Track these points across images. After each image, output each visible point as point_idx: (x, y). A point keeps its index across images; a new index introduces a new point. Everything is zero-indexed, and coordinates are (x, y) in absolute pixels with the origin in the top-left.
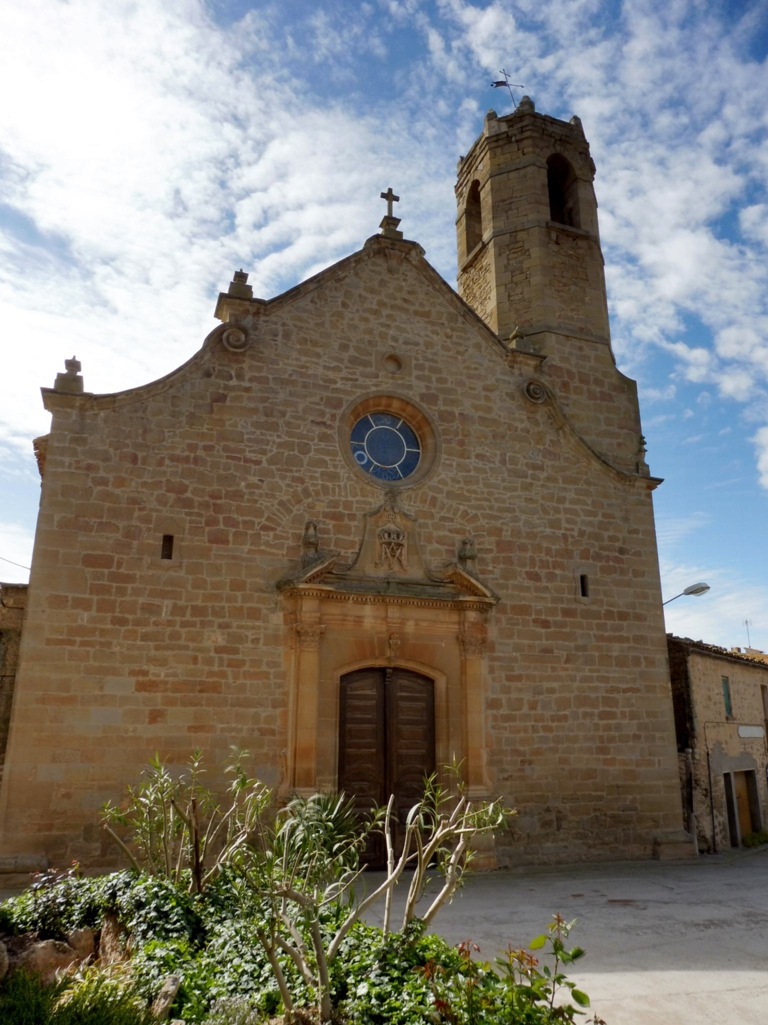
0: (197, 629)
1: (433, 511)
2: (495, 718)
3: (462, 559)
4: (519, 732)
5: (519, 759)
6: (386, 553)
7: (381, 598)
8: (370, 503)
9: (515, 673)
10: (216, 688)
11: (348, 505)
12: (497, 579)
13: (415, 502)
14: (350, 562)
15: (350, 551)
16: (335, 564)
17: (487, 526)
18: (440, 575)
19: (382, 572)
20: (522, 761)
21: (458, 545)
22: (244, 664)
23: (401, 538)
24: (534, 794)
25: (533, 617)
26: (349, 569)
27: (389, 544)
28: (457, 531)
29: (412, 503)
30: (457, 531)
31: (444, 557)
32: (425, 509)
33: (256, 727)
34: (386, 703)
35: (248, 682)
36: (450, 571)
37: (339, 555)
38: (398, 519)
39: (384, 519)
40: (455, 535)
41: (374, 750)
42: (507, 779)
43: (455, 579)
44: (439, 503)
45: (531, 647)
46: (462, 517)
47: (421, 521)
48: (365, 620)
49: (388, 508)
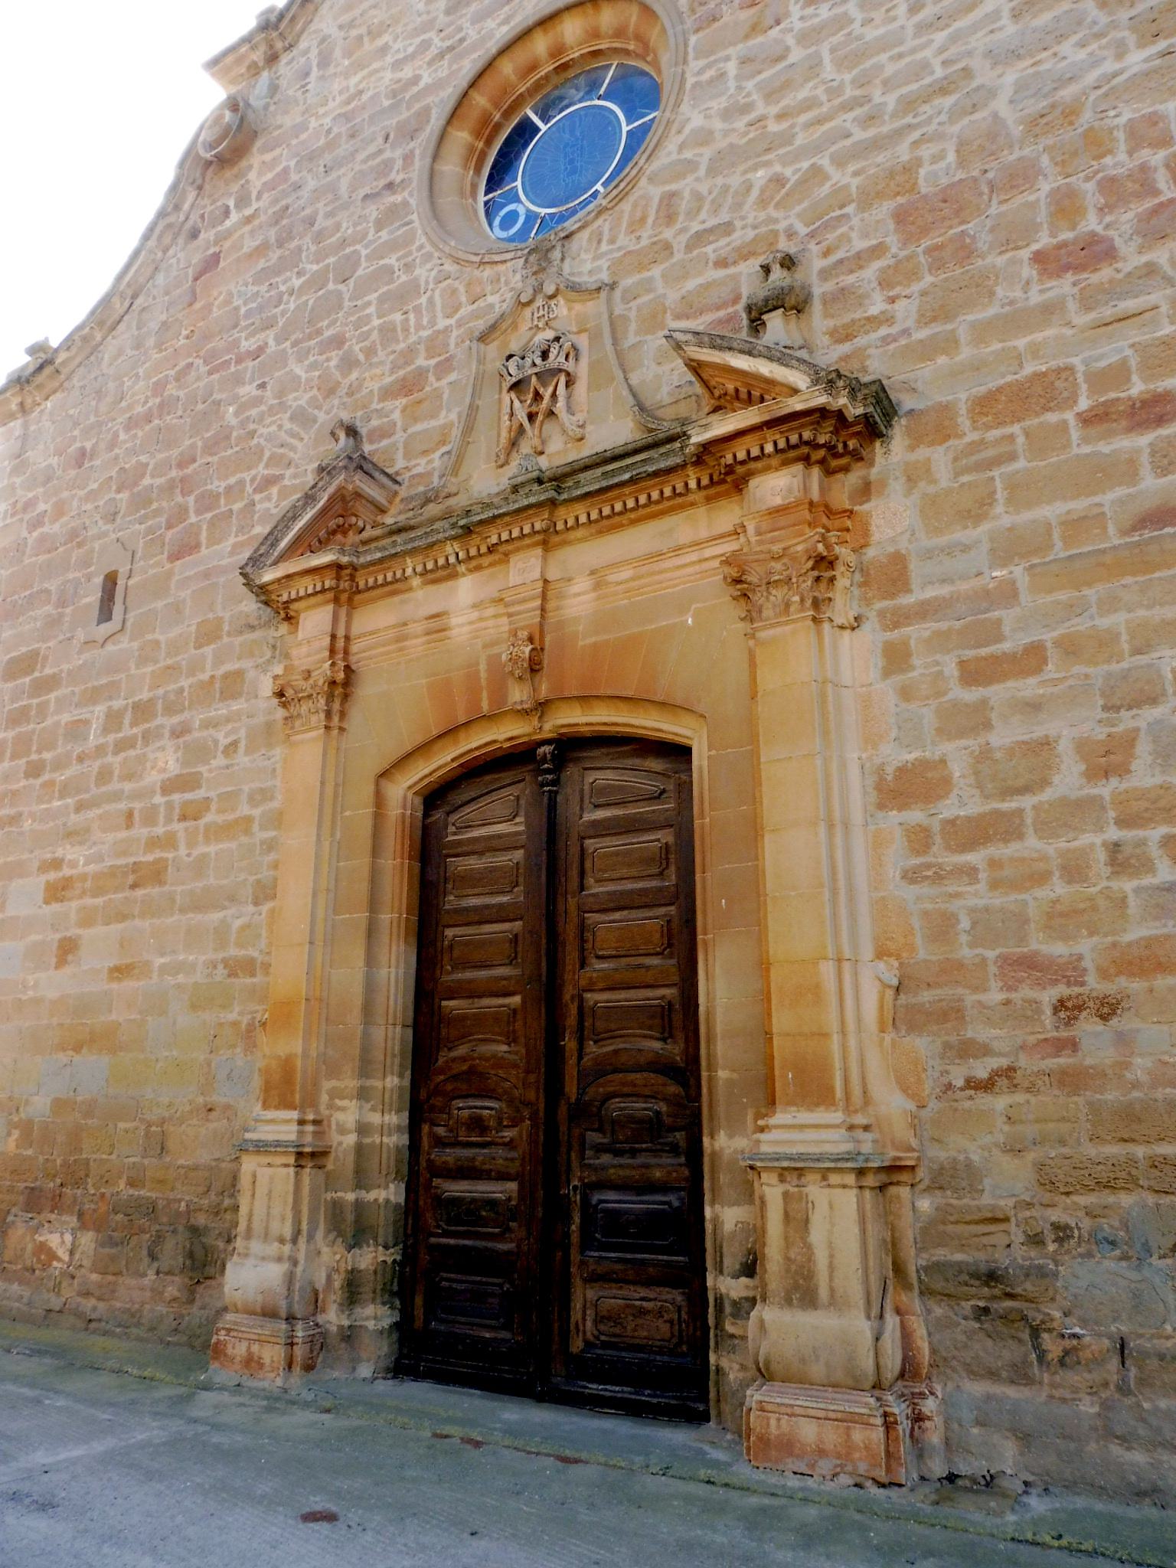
0: (139, 752)
2: (919, 839)
4: (1041, 878)
5: (1048, 996)
9: (1006, 646)
10: (156, 874)
12: (906, 332)
17: (855, 182)
20: (1060, 1005)
22: (208, 809)
24: (1140, 1151)
25: (1084, 404)
33: (220, 955)
34: (554, 856)
35: (212, 849)
41: (516, 1000)
42: (986, 1086)
45: (1075, 526)
48: (454, 621)
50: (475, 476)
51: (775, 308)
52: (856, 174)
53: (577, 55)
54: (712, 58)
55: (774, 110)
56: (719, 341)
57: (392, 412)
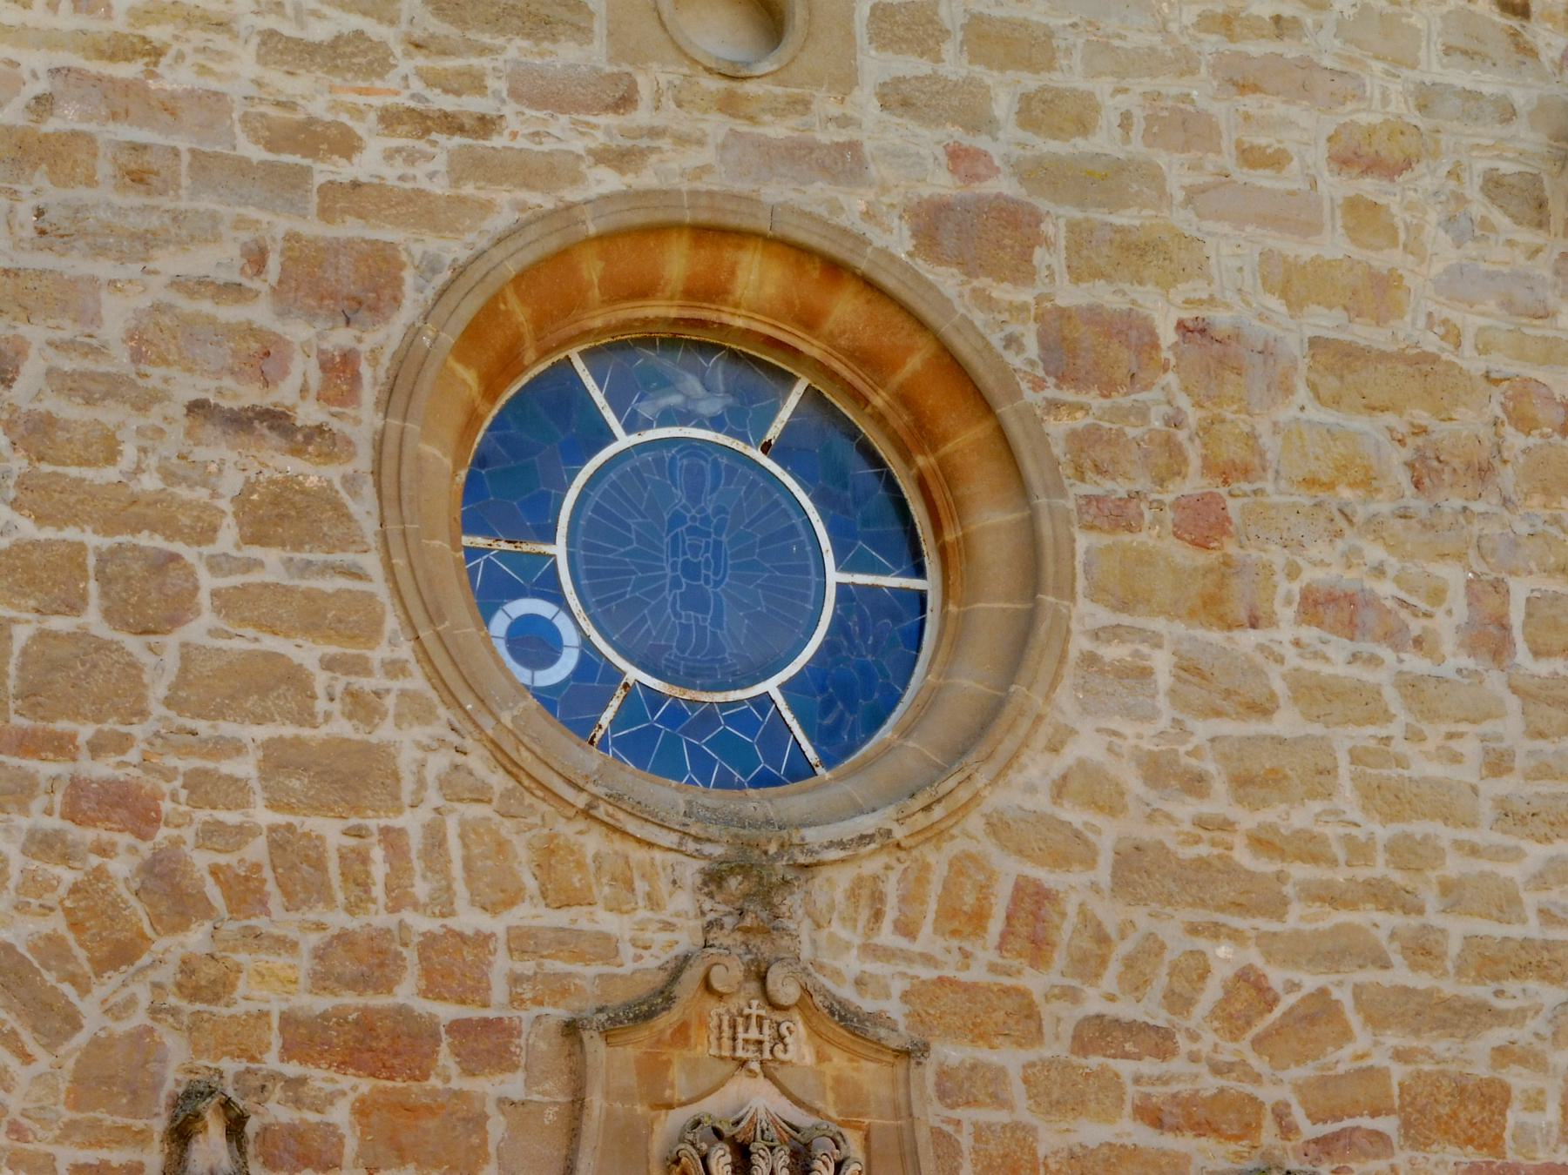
1: (1034, 982)
8: (606, 947)
11: (453, 965)
13: (907, 929)
29: (887, 936)
32: (976, 974)
38: (800, 1048)
39: (705, 1047)
40: (1183, 1143)
46: (1231, 1020)
47: (950, 1052)
49: (728, 975)
52: (1400, 1055)
53: (739, 323)
54: (1125, 619)
55: (1248, 820)
57: (331, 1099)
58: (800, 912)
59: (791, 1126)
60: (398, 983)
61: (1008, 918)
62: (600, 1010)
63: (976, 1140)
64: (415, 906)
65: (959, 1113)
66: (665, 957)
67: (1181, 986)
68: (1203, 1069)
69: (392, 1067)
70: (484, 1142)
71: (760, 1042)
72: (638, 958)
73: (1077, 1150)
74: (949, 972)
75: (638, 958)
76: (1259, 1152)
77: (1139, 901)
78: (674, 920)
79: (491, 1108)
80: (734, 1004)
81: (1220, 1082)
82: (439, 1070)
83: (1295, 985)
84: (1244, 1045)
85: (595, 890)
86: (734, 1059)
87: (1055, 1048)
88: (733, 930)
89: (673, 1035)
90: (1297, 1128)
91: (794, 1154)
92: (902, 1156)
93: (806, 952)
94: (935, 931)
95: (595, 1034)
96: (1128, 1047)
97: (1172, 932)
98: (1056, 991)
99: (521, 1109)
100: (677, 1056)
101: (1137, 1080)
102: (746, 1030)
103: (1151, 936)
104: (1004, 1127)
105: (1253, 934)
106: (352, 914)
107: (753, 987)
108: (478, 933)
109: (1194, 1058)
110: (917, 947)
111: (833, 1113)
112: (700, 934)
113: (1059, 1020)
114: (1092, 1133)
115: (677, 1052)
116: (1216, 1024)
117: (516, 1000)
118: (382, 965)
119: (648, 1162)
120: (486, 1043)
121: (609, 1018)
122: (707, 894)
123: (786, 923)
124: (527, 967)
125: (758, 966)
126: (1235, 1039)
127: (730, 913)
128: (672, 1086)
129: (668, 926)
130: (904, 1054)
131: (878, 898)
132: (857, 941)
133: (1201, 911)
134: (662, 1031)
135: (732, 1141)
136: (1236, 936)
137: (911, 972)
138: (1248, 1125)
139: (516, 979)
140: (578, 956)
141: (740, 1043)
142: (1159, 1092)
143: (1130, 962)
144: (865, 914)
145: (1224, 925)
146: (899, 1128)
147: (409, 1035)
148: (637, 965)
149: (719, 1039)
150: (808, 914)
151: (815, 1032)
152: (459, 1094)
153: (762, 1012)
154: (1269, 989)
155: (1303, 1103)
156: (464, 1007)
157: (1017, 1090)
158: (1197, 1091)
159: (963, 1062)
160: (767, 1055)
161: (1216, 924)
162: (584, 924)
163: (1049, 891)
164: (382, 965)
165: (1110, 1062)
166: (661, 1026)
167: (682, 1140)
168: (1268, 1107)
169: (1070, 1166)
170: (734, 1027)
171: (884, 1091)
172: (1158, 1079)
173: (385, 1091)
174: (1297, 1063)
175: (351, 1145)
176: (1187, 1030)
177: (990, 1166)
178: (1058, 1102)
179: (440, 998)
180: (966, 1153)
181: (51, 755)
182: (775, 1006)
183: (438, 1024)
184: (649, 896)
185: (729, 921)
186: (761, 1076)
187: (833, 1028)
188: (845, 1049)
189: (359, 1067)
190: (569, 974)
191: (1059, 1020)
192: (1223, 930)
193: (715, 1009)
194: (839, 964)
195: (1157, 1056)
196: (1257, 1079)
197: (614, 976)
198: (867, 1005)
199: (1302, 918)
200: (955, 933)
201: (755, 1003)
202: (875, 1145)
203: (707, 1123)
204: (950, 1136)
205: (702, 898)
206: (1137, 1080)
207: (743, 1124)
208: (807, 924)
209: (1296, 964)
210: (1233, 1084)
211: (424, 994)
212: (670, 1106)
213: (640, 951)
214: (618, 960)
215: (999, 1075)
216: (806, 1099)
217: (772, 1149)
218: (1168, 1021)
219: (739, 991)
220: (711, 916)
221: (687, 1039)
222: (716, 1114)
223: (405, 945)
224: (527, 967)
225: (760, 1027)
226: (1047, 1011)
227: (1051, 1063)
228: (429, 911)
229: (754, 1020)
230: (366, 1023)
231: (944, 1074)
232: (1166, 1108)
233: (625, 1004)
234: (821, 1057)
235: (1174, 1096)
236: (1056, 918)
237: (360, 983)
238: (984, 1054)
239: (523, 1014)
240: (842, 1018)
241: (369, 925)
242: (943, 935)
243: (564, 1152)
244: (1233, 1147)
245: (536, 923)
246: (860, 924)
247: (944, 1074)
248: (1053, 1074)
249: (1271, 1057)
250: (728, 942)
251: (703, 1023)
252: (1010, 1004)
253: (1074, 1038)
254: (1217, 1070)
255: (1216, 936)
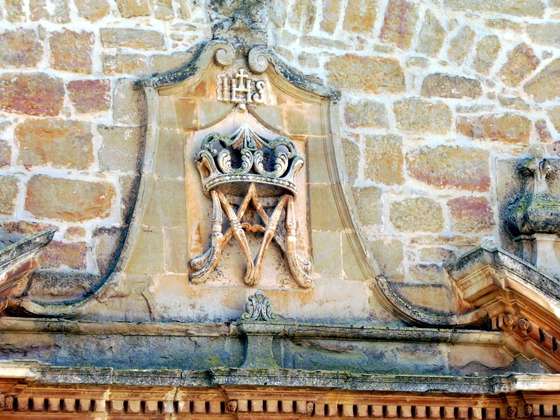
1: (400, 55)
3: (519, 232)
6: (227, 225)
7: (213, 397)
8: (157, 40)
11: (69, 48)
13: (328, 27)
14: (91, 267)
15: (90, 225)
16: (35, 275)
18: (437, 301)
19: (215, 298)
21: (501, 180)
23: (282, 167)
26: (89, 294)
27: (239, 190)
28: (494, 130)
29: (316, 31)
30: (494, 130)
31: (447, 230)
32: (368, 52)
36: (476, 282)
37: (48, 240)
38: (268, 96)
39: (215, 96)
40: (485, 145)
43: (494, 311)
44: (418, 27)
46: (512, 74)
47: (353, 97)
49: (227, 55)
50: (156, 283)
51: (550, 232)
56: (550, 286)
58: (267, 19)
59: (264, 139)
60: (39, 60)
61: (385, 19)
62: (154, 75)
63: (367, 146)
64: (47, 17)
65: (358, 131)
66: (190, 45)
67: (484, 56)
68: (496, 103)
69: (37, 108)
70: (91, 150)
71: (246, 93)
72: (175, 46)
73: (425, 150)
74: (352, 51)
75: (175, 46)
76: (528, 148)
77: (460, 8)
78: (195, 24)
79: (94, 131)
80: (230, 72)
81: (506, 110)
82: (64, 110)
83: (548, 54)
84: (520, 88)
85: (150, 7)
86: (231, 102)
87: (412, 92)
88: (229, 30)
89: (196, 89)
90: (550, 135)
91: (266, 155)
92: (326, 155)
93: (271, 41)
94: (344, 28)
95: (152, 89)
96: (453, 91)
97: (479, 26)
98: (413, 60)
99: (111, 131)
100: (198, 100)
101: (459, 109)
102: (238, 86)
103: (466, 28)
104: (383, 138)
105: (525, 25)
106: (11, 21)
107: (241, 61)
108: (83, 32)
109: (491, 96)
110: (334, 37)
111: (287, 132)
112: (210, 32)
113: (414, 77)
114: (433, 140)
115: (198, 99)
116: (504, 77)
117: (106, 70)
118: (29, 50)
119: (184, 160)
120: (90, 94)
121: (160, 80)
122: (213, 9)
123: (259, 25)
124: (112, 51)
125: (244, 50)
126: (514, 86)
127: (227, 20)
128: (197, 118)
129: (192, 27)
130: (327, 98)
131: (311, 10)
132: (300, 34)
133: (495, 13)
134: (190, 87)
135: (231, 148)
136: (515, 27)
137: (330, 52)
138: (522, 134)
139: (106, 58)
140: (140, 45)
141: (234, 93)
142: (471, 116)
143: (454, 43)
144: (304, 19)
145: (508, 21)
146: (324, 140)
147: (46, 90)
148: (175, 50)
149: (223, 91)
150: (271, 20)
151: (276, 87)
152: (75, 123)
153: (247, 76)
154: (534, 56)
155: (553, 121)
156: (77, 74)
157: (391, 116)
158: (493, 115)
159: (360, 102)
160: (249, 100)
161: (504, 20)
162: (143, 27)
163: (409, 3)
164: (29, 50)
165: (444, 100)
166: (189, 84)
167: (202, 148)
168: (533, 123)
169: (420, 158)
170: (230, 84)
171: (316, 119)
172: (471, 108)
173: (34, 122)
174: (550, 99)
175: (15, 152)
176: (487, 80)
177: (375, 159)
178: (414, 123)
179: (63, 69)
180: (362, 152)
181: (122, 183)
182: (253, 72)
183: (62, 84)
184: (180, 11)
185: (226, 25)
186: (246, 112)
187: (286, 84)
188: (294, 96)
189: (19, 108)
190: (136, 55)
191: (414, 77)
192: (508, 24)
193: (219, 74)
194: (290, 48)
195: (470, 96)
196: (527, 107)
197: (162, 56)
198: (306, 71)
199: (552, 16)
200: (355, 29)
201: (242, 71)
202: (311, 149)
203: (217, 138)
204: (353, 143)
205: (211, 11)
206: (459, 109)
207: (237, 138)
208: (271, 25)
209: (549, 42)
210: (513, 111)
211: (55, 66)
212: (195, 129)
213: (177, 42)
214: (164, 47)
215: (381, 108)
216: (272, 124)
217: (253, 152)
218: (476, 76)
219: (233, 64)
220: (216, 22)
221: (204, 91)
222: (221, 134)
223: (42, 39)
224: (112, 51)
225: (246, 85)
226: (407, 72)
227: (410, 101)
228: (55, 20)
229: (242, 80)
230: (21, 85)
231: (349, 109)
232: (475, 125)
233: (168, 72)
234: (280, 101)
235: (480, 118)
236: (413, 20)
237: (18, 60)
238: (371, 97)
239: (111, 78)
240: (292, 79)
241: (21, 28)
242: (348, 30)
243: (136, 155)
244: (513, 146)
245: (117, 26)
246: (301, 25)
247: (349, 109)
248: (411, 107)
249: (535, 95)
250: (226, 36)
251: (213, 82)
252: (386, 68)
253: (423, 87)
254: (504, 103)
255: (504, 27)
